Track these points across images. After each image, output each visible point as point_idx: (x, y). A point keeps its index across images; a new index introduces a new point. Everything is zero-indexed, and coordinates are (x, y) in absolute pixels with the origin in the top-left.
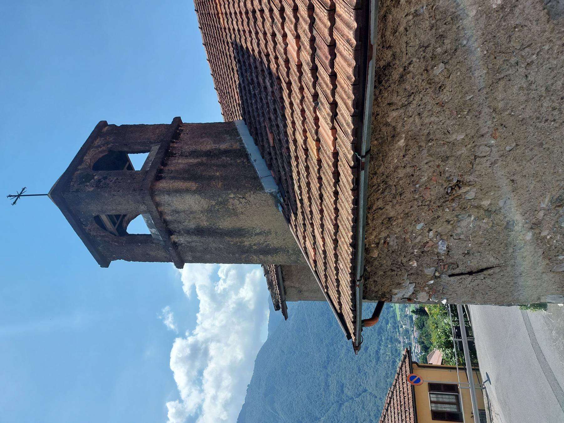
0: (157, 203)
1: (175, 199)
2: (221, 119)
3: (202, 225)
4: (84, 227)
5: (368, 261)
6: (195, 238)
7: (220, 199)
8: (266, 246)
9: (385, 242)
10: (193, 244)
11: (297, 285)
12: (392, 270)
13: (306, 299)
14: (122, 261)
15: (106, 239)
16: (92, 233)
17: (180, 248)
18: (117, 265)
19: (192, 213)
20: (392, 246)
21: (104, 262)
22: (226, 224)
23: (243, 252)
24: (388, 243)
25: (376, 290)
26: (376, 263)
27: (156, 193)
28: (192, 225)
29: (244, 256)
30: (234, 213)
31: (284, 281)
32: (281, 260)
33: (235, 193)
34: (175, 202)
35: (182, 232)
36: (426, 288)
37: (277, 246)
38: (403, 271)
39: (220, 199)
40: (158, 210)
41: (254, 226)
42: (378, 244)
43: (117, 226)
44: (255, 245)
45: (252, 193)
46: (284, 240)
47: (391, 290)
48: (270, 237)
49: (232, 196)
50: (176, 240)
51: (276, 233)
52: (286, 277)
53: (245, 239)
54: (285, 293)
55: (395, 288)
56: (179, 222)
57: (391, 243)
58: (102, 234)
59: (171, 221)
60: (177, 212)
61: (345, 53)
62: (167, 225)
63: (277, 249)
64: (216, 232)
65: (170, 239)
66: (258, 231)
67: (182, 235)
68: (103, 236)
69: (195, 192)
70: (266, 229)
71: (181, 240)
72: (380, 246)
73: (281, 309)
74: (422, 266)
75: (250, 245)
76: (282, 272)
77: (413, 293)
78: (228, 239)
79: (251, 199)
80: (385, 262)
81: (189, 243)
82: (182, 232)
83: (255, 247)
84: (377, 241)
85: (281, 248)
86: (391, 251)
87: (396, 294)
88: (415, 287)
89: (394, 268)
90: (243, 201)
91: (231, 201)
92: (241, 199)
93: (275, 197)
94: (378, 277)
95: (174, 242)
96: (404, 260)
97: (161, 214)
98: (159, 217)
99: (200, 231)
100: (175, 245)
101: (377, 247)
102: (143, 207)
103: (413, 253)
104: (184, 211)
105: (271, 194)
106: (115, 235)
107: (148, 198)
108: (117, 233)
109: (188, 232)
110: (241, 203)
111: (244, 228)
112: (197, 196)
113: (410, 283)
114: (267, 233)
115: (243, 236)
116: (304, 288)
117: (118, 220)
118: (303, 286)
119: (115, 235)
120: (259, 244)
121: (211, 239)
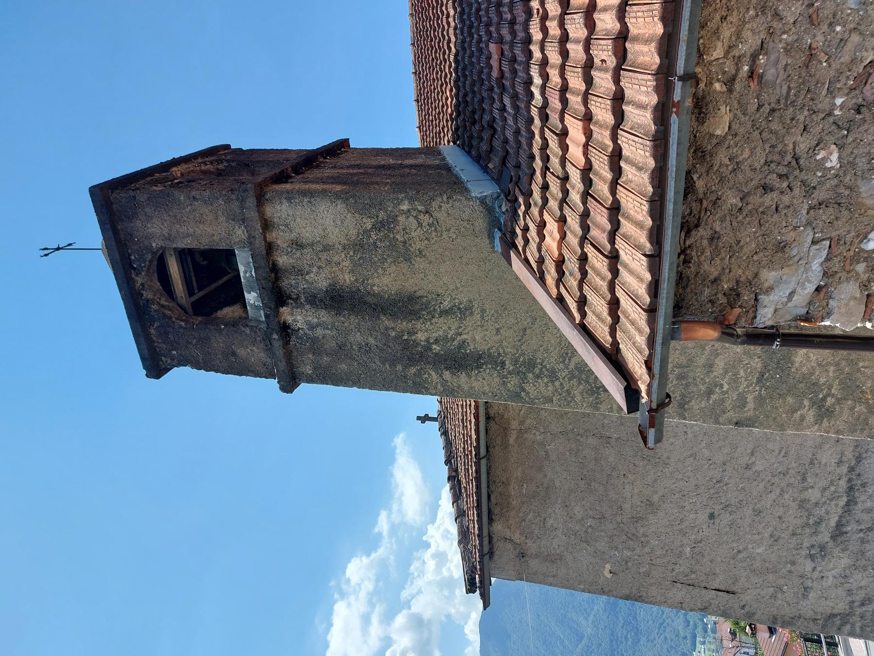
0: (266, 220)
1: (299, 211)
2: (414, 141)
3: (341, 282)
4: (133, 276)
5: (700, 152)
6: (324, 316)
7: (382, 215)
8: (460, 347)
9: (751, 75)
10: (319, 332)
11: (517, 537)
12: (766, 189)
13: (532, 578)
14: (187, 369)
15: (168, 312)
16: (144, 293)
17: (293, 340)
18: (182, 377)
19: (326, 248)
20: (773, 84)
21: (156, 368)
22: (386, 281)
23: (412, 360)
24: (761, 77)
25: (714, 273)
26: (722, 157)
27: (267, 197)
28: (320, 280)
29: (413, 370)
30: (404, 254)
31: (491, 520)
32: (487, 388)
33: (411, 200)
34: (298, 220)
35: (303, 300)
36: (861, 267)
37: (482, 347)
38: (797, 191)
39: (382, 215)
40: (265, 238)
41: (440, 291)
42: (730, 82)
43: (194, 299)
44: (437, 341)
45: (445, 198)
46: (498, 331)
47: (756, 275)
48: (469, 322)
49: (405, 207)
50: (289, 319)
51: (483, 311)
52: (496, 510)
53: (419, 325)
54: (491, 553)
55: (771, 265)
56: (300, 272)
57: (770, 75)
58: (163, 302)
59: (286, 270)
60: (298, 245)
61: (633, 316)
62: (277, 279)
63: (480, 357)
64: (365, 303)
65: (277, 314)
66: (446, 304)
67: (301, 306)
68: (163, 306)
69: (337, 196)
70: (463, 298)
71: (297, 317)
72: (738, 86)
73: (478, 592)
74: (852, 164)
75: (427, 340)
76: (489, 496)
77: (818, 289)
78: (386, 321)
79: (441, 216)
80: (747, 153)
81: (312, 327)
82: (303, 300)
83: (436, 348)
84: (729, 67)
85: (489, 355)
86: (766, 109)
87: (770, 289)
88: (828, 259)
89: (773, 179)
90: (425, 219)
91: (401, 219)
92: (421, 216)
93: (490, 210)
94: (722, 220)
95: (285, 323)
96: (804, 144)
97: (270, 247)
98: (264, 252)
99: (336, 300)
100: (285, 330)
101: (730, 91)
102: (239, 232)
103: (830, 114)
104: (312, 245)
105: (482, 201)
106: (186, 312)
107: (251, 202)
108: (190, 311)
109: (314, 300)
110: (420, 225)
111: (418, 294)
112: (340, 206)
113: (814, 242)
114: (461, 311)
115: (415, 315)
116: (531, 547)
117: (199, 290)
118: (530, 543)
119: (186, 312)
120: (445, 339)
121: (354, 320)
